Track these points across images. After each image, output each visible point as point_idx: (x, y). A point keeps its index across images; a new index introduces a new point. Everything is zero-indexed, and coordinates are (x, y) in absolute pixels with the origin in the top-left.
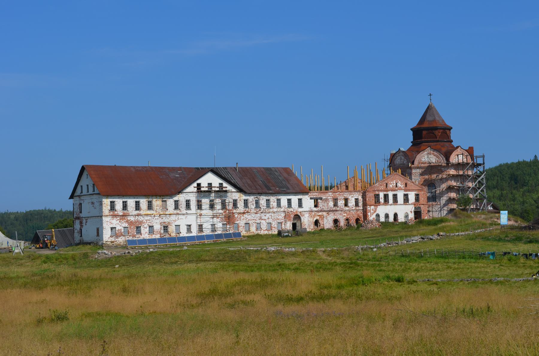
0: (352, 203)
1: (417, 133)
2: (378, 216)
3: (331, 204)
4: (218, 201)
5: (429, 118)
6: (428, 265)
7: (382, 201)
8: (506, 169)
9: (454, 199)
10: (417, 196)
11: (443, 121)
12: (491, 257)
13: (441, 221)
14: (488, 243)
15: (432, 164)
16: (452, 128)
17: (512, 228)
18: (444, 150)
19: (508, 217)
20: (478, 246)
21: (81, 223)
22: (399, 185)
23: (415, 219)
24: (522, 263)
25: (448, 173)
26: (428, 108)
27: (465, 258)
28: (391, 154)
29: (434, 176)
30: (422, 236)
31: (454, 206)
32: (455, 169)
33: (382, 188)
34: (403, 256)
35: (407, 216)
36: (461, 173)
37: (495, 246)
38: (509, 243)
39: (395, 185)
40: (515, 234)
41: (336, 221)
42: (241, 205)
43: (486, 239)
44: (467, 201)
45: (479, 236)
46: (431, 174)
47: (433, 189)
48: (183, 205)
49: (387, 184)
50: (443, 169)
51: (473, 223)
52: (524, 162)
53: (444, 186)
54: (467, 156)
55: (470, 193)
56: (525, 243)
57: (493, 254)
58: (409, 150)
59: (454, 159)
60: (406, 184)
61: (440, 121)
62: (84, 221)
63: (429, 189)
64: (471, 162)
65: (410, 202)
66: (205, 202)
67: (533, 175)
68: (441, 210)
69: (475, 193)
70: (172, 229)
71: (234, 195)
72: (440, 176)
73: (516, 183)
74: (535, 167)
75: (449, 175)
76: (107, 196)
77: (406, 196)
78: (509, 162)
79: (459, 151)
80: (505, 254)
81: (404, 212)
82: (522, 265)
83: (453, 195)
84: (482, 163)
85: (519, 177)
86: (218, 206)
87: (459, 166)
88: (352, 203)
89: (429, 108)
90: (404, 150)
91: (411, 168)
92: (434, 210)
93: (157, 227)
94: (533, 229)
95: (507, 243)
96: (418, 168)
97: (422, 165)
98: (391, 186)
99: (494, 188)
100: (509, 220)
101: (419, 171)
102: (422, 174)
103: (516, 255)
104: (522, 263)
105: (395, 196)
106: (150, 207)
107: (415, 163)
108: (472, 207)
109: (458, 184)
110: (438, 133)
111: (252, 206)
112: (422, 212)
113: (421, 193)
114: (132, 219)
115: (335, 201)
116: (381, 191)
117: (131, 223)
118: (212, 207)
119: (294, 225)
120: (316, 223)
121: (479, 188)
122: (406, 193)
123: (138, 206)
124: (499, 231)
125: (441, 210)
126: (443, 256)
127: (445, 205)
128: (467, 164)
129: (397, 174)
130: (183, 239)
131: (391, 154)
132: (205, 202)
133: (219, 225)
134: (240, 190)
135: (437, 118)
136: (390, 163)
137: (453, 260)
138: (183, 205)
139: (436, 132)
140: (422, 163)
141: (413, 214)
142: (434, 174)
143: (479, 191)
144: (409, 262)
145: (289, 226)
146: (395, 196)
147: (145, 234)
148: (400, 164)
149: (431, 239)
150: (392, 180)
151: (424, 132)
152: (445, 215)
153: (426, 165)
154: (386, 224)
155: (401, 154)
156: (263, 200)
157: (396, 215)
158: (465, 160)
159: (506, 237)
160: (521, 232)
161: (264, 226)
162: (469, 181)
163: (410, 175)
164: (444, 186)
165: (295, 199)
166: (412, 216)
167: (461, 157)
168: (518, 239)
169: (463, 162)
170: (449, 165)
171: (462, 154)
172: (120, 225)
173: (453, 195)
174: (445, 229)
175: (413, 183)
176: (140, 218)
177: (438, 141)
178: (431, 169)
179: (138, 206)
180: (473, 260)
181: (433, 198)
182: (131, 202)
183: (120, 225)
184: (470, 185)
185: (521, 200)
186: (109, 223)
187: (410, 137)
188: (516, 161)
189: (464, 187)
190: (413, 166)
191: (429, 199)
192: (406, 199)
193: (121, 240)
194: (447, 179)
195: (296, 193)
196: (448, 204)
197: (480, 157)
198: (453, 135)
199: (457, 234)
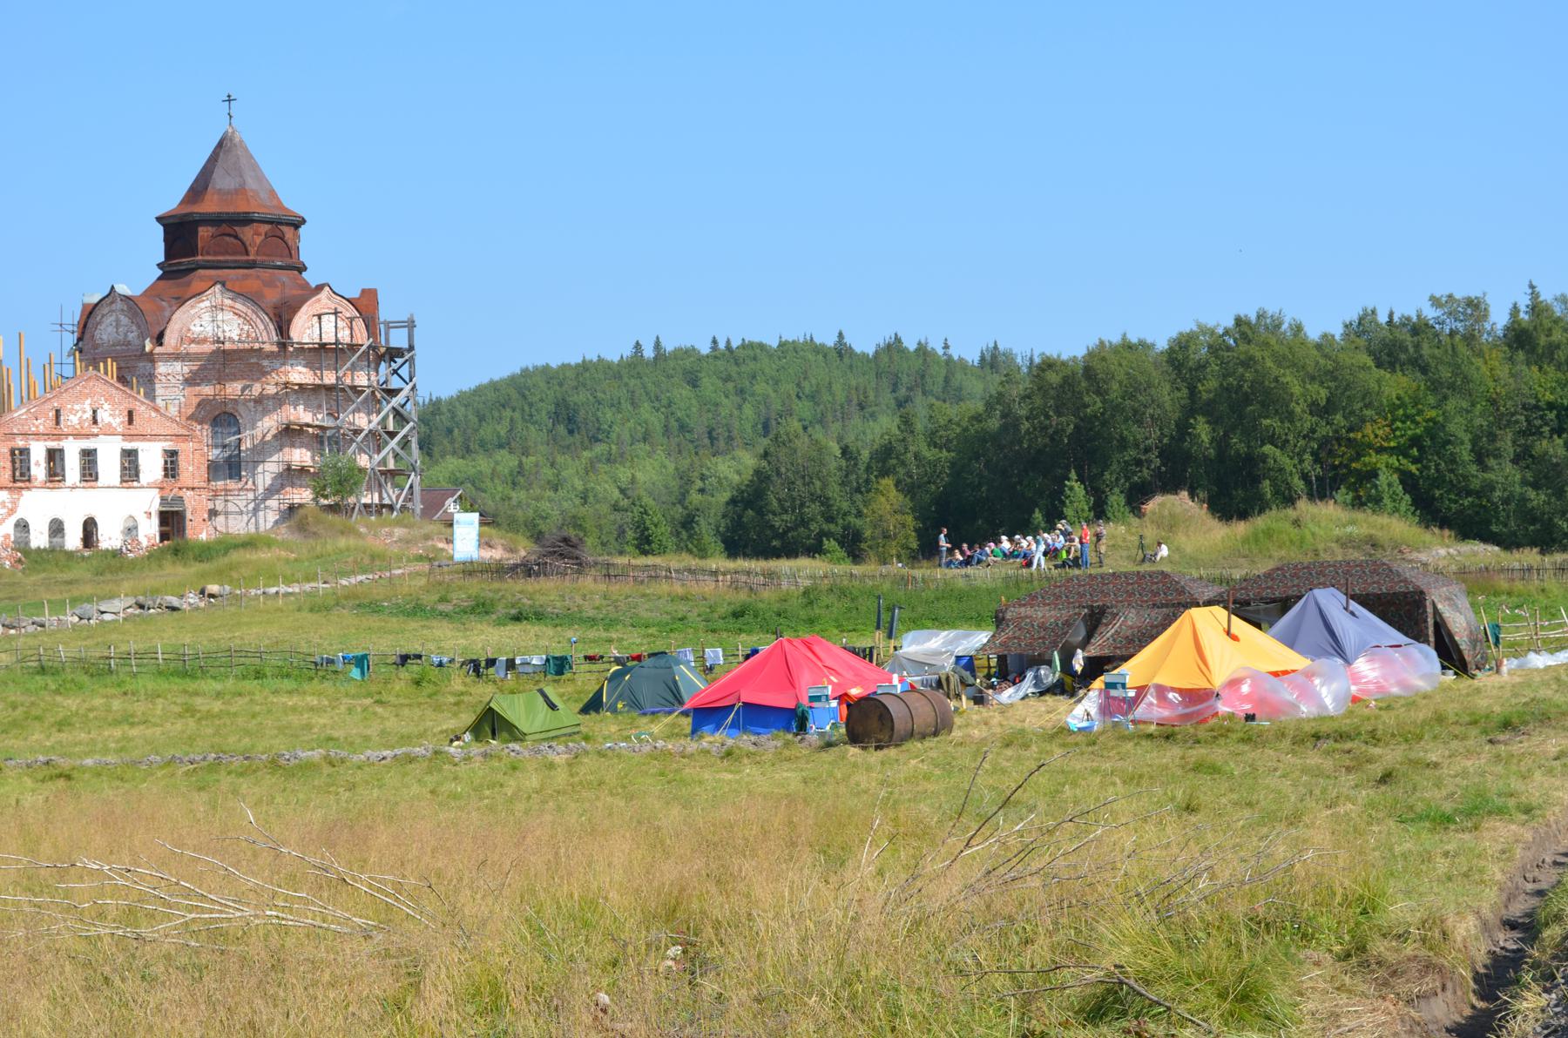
1: (180, 233)
2: (22, 526)
5: (221, 181)
6: (116, 704)
7: (39, 470)
8: (542, 385)
9: (303, 470)
10: (172, 455)
11: (273, 193)
12: (355, 673)
13: (250, 543)
14: (374, 621)
15: (228, 346)
16: (304, 221)
17: (498, 571)
18: (272, 296)
19: (480, 535)
20: (332, 636)
22: (103, 416)
23: (162, 540)
24: (453, 694)
25: (284, 379)
26: (220, 145)
27: (265, 676)
28: (85, 306)
29: (234, 388)
30: (141, 599)
31: (302, 495)
32: (308, 365)
33: (43, 424)
34: (42, 670)
35: (131, 530)
36: (329, 378)
37: (390, 632)
38: (445, 623)
39: (89, 414)
40: (473, 591)
43: (368, 606)
44: (346, 480)
45: (346, 598)
46: (221, 380)
47: (230, 435)
49: (58, 412)
50: (265, 363)
51: (341, 551)
52: (602, 366)
53: (269, 424)
54: (351, 319)
55: (361, 450)
56: (499, 623)
57: (360, 662)
58: (150, 292)
59: (304, 329)
60: (130, 414)
61: (263, 195)
63: (215, 433)
64: (367, 343)
65: (145, 477)
67: (626, 406)
68: (256, 510)
69: (379, 452)
72: (256, 389)
73: (571, 432)
74: (633, 382)
75: (286, 385)
78: (554, 364)
79: (324, 301)
80: (404, 659)
81: (125, 514)
82: (452, 699)
83: (300, 456)
84: (405, 345)
85: (582, 412)
87: (322, 353)
89: (223, 146)
90: (128, 292)
91: (151, 358)
92: (231, 507)
94: (538, 574)
95: (435, 623)
96: (177, 357)
97: (194, 348)
98: (74, 420)
99: (501, 446)
100: (485, 543)
101: (180, 369)
102: (190, 381)
103: (440, 665)
104: (453, 694)
105: (89, 457)
107: (166, 339)
108: (366, 500)
109: (321, 419)
110: (253, 236)
112: (189, 516)
113: (186, 448)
116: (37, 435)
121: (392, 435)
122: (129, 446)
124: (423, 581)
125: (256, 510)
126: (186, 668)
127: (271, 492)
128: (353, 348)
129: (98, 378)
131: (85, 306)
135: (251, 184)
136: (79, 339)
137: (218, 686)
139: (247, 233)
140: (193, 341)
141: (155, 521)
142: (234, 378)
143: (393, 443)
144: (57, 692)
146: (89, 457)
148: (115, 342)
149: (174, 609)
150: (80, 398)
151: (204, 232)
152: (269, 525)
153: (208, 348)
154: (55, 555)
155: (119, 305)
157: (90, 527)
158: (344, 336)
159: (443, 600)
160: (496, 585)
162: (358, 410)
163: (149, 380)
164: (269, 424)
166: (149, 530)
167: (329, 322)
168: (481, 608)
169: (337, 342)
170: (285, 348)
171: (336, 313)
173: (300, 456)
174: (235, 575)
175: (157, 410)
177: (252, 265)
178: (223, 362)
180: (288, 684)
184: (361, 421)
185: (579, 485)
187: (154, 246)
188: (575, 359)
189: (338, 428)
190: (158, 350)
191: (214, 470)
192: (130, 467)
194: (279, 401)
196: (283, 486)
197: (399, 325)
198: (309, 245)
199: (273, 590)
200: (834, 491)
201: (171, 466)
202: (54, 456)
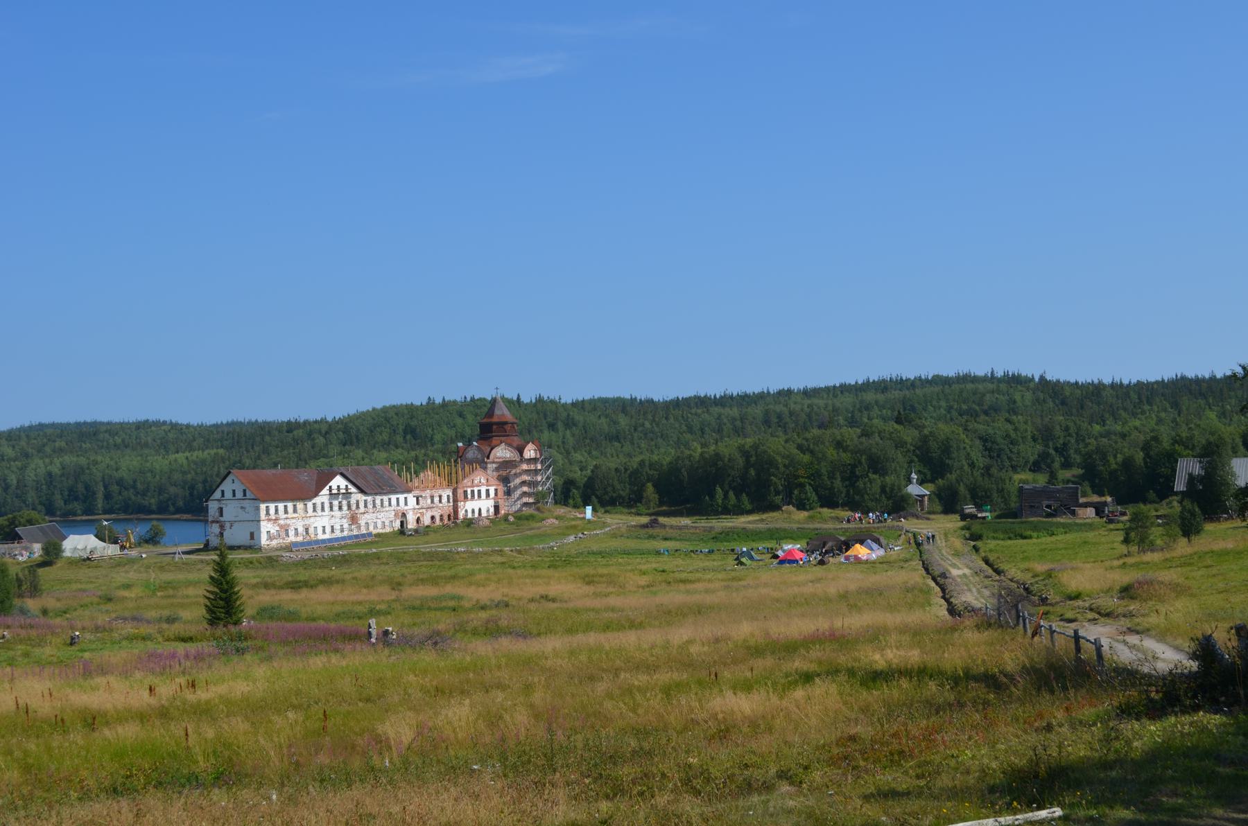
0: (445, 499)
3: (429, 501)
4: (344, 502)
21: (222, 527)
41: (433, 518)
42: (362, 505)
48: (319, 507)
53: (518, 481)
62: (228, 525)
66: (336, 503)
70: (311, 531)
71: (357, 497)
76: (264, 501)
77: (488, 491)
83: (525, 489)
86: (345, 508)
87: (530, 461)
88: (445, 499)
93: (301, 530)
106: (295, 511)
111: (370, 506)
114: (282, 522)
115: (432, 497)
117: (281, 526)
118: (340, 508)
119: (402, 523)
120: (418, 520)
123: (286, 512)
130: (317, 542)
132: (336, 503)
133: (346, 526)
134: (362, 491)
138: (319, 507)
145: (397, 525)
146: (479, 491)
147: (292, 538)
156: (378, 498)
161: (379, 525)
164: (518, 481)
165: (401, 497)
166: (492, 510)
172: (273, 529)
173: (525, 489)
176: (288, 522)
178: (506, 464)
179: (286, 512)
181: (508, 493)
182: (281, 506)
183: (273, 529)
184: (539, 478)
186: (266, 527)
193: (274, 543)
194: (520, 474)
195: (403, 492)
200: (616, 483)
201: (496, 494)
202: (473, 492)
